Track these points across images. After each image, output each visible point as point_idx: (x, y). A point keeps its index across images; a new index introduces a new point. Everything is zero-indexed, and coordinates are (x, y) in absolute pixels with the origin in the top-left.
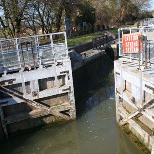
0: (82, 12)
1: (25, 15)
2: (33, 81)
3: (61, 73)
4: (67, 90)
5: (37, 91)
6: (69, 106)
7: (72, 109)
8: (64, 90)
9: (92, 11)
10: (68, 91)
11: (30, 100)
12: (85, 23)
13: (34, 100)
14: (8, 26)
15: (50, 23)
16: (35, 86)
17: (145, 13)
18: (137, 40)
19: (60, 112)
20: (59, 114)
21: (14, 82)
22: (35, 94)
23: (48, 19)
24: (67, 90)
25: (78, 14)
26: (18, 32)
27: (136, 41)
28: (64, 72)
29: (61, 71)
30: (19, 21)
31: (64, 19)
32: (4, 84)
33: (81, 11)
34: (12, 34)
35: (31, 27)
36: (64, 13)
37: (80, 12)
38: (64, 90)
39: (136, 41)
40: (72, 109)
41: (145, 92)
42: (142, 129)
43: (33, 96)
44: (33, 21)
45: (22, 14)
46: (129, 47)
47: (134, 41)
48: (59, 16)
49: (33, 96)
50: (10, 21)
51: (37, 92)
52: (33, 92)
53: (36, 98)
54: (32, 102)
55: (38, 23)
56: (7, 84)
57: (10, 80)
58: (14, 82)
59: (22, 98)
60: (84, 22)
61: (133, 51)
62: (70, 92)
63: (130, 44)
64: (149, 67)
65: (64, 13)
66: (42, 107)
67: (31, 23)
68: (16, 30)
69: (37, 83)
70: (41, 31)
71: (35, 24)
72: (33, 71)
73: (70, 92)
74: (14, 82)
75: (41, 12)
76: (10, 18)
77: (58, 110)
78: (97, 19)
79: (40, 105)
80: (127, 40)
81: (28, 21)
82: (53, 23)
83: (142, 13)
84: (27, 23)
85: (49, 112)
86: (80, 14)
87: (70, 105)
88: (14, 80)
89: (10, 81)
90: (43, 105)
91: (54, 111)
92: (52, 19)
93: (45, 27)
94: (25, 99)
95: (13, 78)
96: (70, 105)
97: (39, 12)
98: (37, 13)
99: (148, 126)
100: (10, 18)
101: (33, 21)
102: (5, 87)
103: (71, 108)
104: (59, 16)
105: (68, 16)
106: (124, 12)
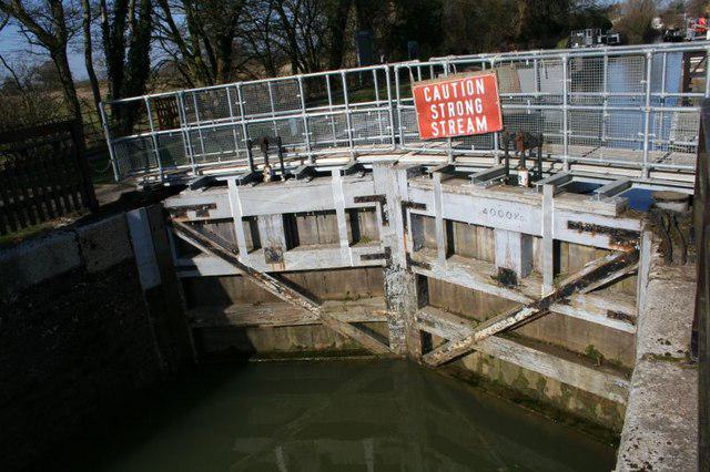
0: (406, 12)
1: (243, 22)
2: (266, 217)
3: (358, 199)
4: (377, 256)
5: (280, 249)
6: (385, 312)
7: (394, 323)
8: (368, 257)
9: (434, 9)
10: (383, 262)
11: (256, 272)
12: (415, 43)
13: (269, 274)
14: (198, 53)
15: (315, 44)
16: (273, 233)
17: (588, 15)
18: (481, 96)
19: (352, 324)
20: (349, 331)
21: (210, 211)
22: (274, 257)
23: (308, 31)
24: (377, 256)
25: (393, 17)
26: (225, 70)
27: (474, 97)
28: (369, 199)
29: (359, 195)
30: (226, 43)
31: (352, 27)
32: (184, 215)
33: (402, 9)
34: (208, 75)
35: (258, 56)
36: (353, 14)
37: (397, 11)
38: (368, 257)
39: (474, 97)
40: (394, 323)
41: (557, 244)
42: (555, 359)
43: (267, 262)
44: (267, 41)
45: (235, 20)
46: (447, 119)
47: (468, 98)
48: (339, 25)
49: (267, 262)
50: (201, 42)
51: (278, 252)
52: (266, 249)
53: (277, 268)
54: (264, 278)
55: (281, 46)
56: (192, 216)
57: (201, 206)
58: (213, 214)
59: (233, 261)
60: (411, 39)
61: (465, 128)
62: (388, 267)
63: (451, 110)
64: (547, 172)
65: (353, 14)
66: (293, 296)
67: (261, 47)
68: (220, 63)
69: (278, 223)
70: (288, 67)
71: (273, 49)
72: (275, 187)
73: (388, 267)
74: (210, 211)
75: (289, 14)
76: (203, 34)
77: (344, 317)
78: (448, 34)
79: (286, 292)
80: (437, 95)
81: (251, 41)
82: (321, 44)
83: (578, 12)
84: (250, 45)
85: (316, 318)
86: (398, 18)
87: (388, 308)
88: (212, 206)
89: (202, 209)
90: (297, 294)
91: (333, 318)
92: (320, 33)
93: (302, 59)
94: (242, 267)
95: (210, 202)
96: (388, 308)
97: (281, 12)
98: (278, 17)
99: (564, 344)
100: (203, 34)
101: (267, 41)
102: (185, 223)
103: (390, 317)
104: (339, 25)
105: (365, 24)
106: (525, 13)
